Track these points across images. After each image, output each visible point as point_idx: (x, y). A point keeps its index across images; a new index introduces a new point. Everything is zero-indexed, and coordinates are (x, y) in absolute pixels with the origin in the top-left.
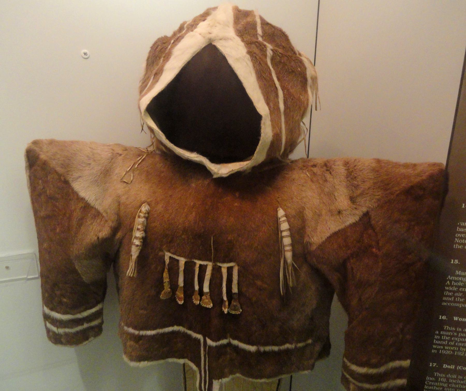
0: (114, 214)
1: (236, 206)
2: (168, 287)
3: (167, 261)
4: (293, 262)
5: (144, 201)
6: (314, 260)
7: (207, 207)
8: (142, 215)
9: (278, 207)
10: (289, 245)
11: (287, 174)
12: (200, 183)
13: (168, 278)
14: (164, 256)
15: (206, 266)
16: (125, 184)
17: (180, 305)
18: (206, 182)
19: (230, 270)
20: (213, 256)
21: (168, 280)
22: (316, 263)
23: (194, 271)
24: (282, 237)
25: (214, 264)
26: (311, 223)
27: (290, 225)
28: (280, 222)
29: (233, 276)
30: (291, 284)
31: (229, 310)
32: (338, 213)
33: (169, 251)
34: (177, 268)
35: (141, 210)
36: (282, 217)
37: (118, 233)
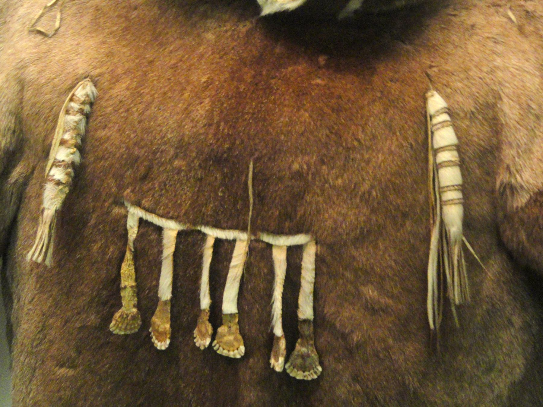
0: (7, 114)
1: (318, 85)
2: (133, 303)
3: (133, 233)
4: (464, 239)
5: (83, 74)
6: (523, 236)
7: (242, 87)
8: (75, 106)
9: (427, 90)
10: (456, 187)
11: (455, 15)
12: (226, 31)
13: (134, 277)
14: (126, 217)
15: (232, 243)
16: (39, 38)
17: (162, 351)
18: (244, 27)
20: (250, 213)
21: (134, 284)
22: (526, 244)
23: (201, 257)
24: (437, 165)
25: (253, 238)
26: (516, 135)
27: (459, 138)
28: (433, 126)
29: (303, 273)
30: (456, 296)
31: (287, 366)
33: (138, 204)
34: (156, 250)
35: (73, 95)
36: (439, 113)
37: (14, 166)
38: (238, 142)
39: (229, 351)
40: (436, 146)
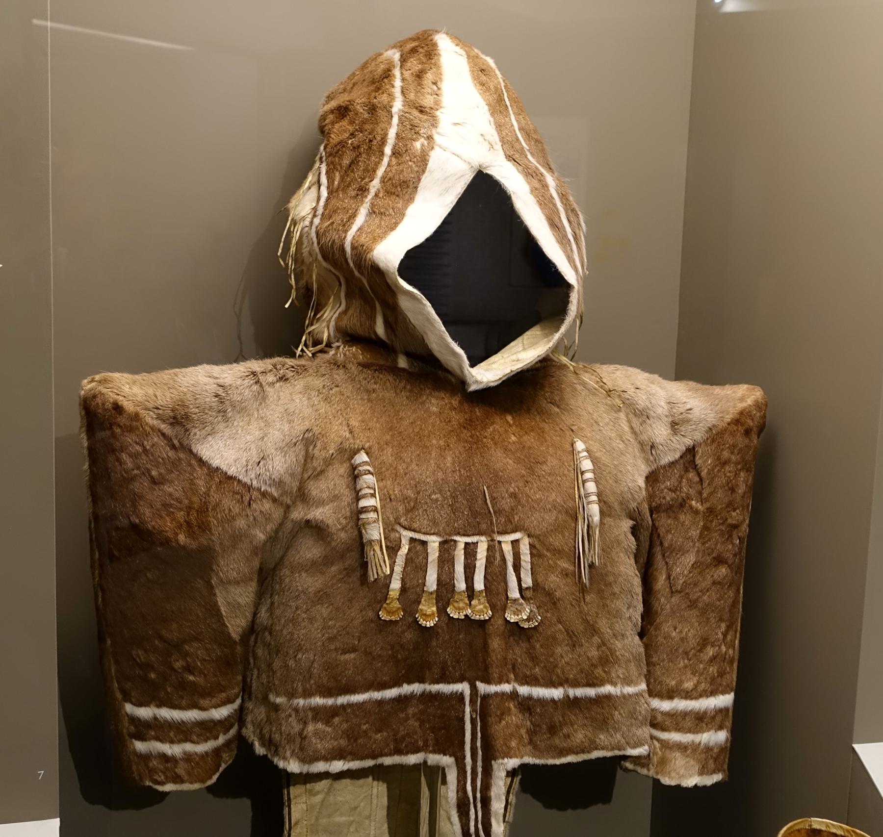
19: (515, 543)
29: (518, 366)
32: (673, 400)
36: (583, 451)
38: (474, 479)
39: (480, 616)
40: (583, 469)
